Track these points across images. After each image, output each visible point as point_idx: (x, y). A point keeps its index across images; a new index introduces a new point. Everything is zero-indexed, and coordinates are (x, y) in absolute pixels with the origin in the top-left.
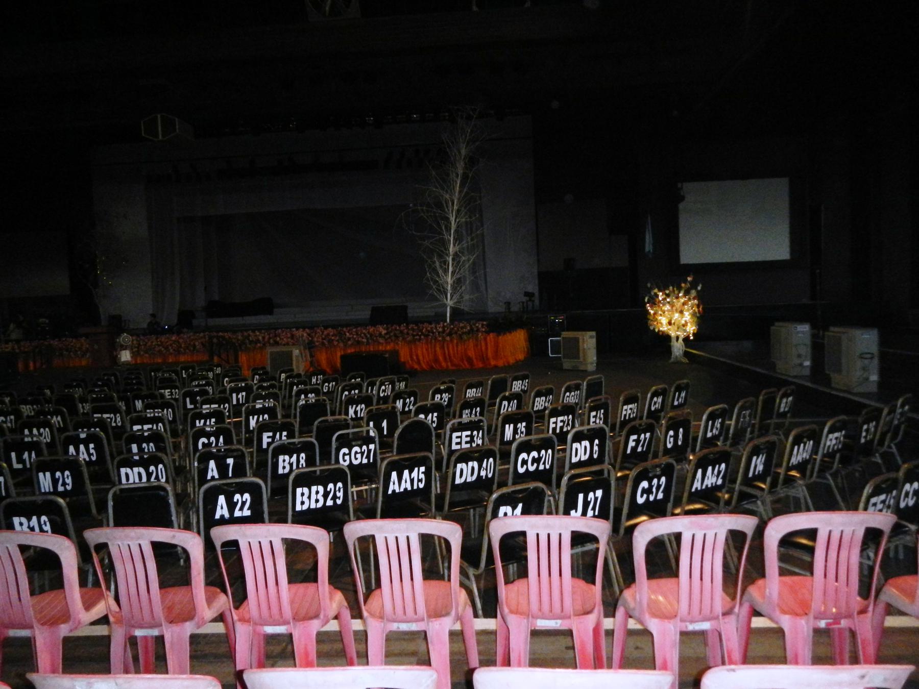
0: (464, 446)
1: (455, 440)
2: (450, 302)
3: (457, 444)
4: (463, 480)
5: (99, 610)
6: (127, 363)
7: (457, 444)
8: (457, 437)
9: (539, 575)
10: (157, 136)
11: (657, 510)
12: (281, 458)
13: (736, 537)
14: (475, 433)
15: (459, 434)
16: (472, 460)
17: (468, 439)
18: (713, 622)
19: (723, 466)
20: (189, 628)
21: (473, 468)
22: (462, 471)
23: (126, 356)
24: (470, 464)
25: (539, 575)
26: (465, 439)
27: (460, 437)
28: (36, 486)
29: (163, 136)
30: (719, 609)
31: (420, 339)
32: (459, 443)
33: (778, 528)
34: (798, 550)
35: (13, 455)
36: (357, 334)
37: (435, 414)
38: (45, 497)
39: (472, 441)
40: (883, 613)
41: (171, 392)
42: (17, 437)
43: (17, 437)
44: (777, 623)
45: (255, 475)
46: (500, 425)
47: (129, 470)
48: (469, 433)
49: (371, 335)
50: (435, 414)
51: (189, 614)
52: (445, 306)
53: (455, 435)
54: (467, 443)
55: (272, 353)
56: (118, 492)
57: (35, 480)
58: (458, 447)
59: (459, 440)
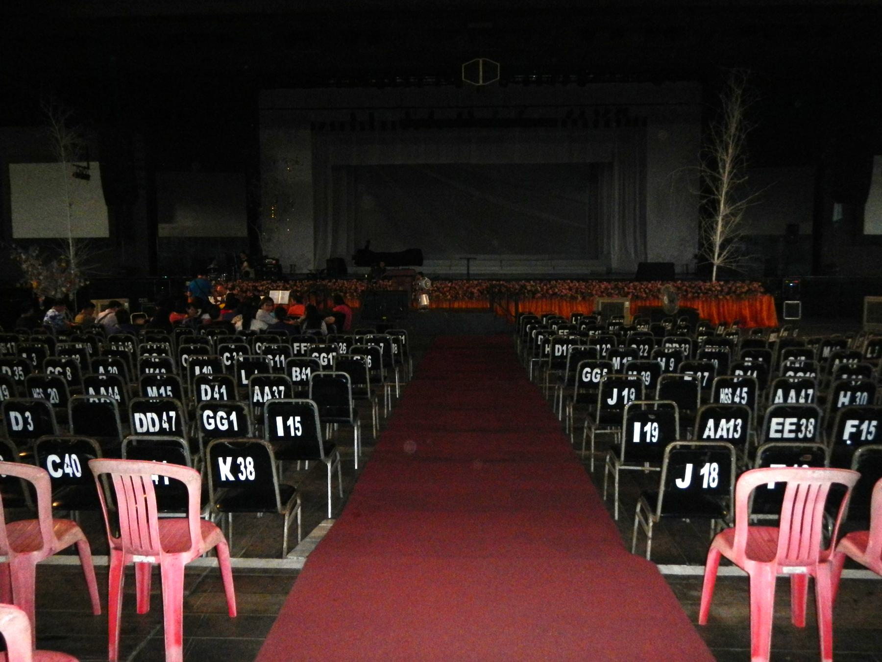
0: (786, 435)
2: (717, 261)
3: (777, 431)
5: (67, 541)
6: (425, 307)
7: (777, 431)
8: (778, 424)
12: (294, 369)
13: (836, 492)
14: (804, 421)
15: (781, 420)
17: (794, 427)
18: (810, 567)
20: (186, 558)
22: (141, 420)
23: (425, 300)
26: (787, 427)
27: (783, 424)
28: (132, 427)
30: (816, 555)
31: (698, 297)
36: (635, 289)
37: (874, 423)
38: (140, 438)
39: (798, 429)
41: (798, 426)
42: (105, 358)
43: (105, 358)
44: (878, 574)
45: (313, 399)
46: (837, 420)
47: (142, 416)
48: (795, 420)
49: (650, 291)
50: (874, 423)
51: (184, 545)
52: (712, 265)
53: (775, 420)
54: (790, 431)
57: (131, 420)
58: (779, 435)
59: (780, 427)
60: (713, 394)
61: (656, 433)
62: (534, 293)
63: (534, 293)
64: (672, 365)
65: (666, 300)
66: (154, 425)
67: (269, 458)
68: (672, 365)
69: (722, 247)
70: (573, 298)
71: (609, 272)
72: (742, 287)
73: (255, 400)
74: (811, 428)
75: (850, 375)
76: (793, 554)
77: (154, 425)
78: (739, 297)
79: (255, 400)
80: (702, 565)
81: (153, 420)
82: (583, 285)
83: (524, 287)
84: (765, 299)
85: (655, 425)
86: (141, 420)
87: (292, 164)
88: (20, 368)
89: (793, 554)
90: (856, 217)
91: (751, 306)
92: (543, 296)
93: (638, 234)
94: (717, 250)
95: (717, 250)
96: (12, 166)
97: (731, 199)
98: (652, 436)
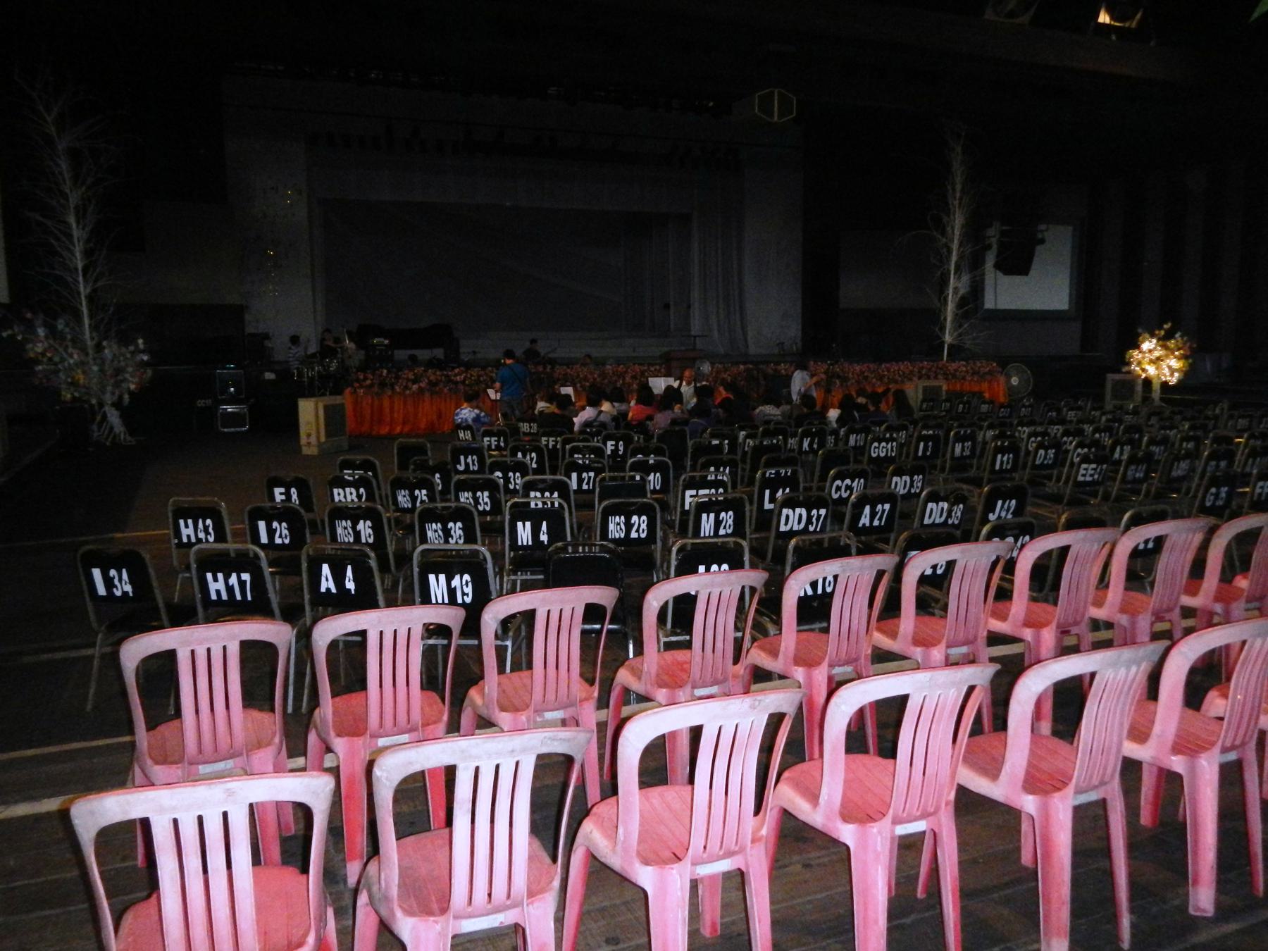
1: (1082, 472)
2: (948, 338)
4: (931, 521)
9: (381, 686)
10: (772, 116)
11: (343, 603)
13: (593, 613)
16: (943, 500)
19: (1014, 502)
21: (800, 516)
22: (787, 517)
24: (798, 510)
25: (381, 686)
29: (780, 116)
32: (1084, 475)
33: (797, 585)
34: (935, 588)
35: (767, 492)
40: (747, 677)
47: (791, 512)
52: (943, 343)
55: (940, 387)
56: (689, 548)
60: (84, 583)
61: (469, 590)
64: (621, 448)
66: (799, 522)
68: (621, 448)
73: (323, 590)
74: (644, 526)
76: (551, 696)
77: (799, 522)
79: (323, 590)
80: (283, 859)
81: (800, 516)
85: (467, 577)
86: (787, 517)
87: (282, 197)
88: (424, 492)
89: (551, 696)
98: (464, 594)
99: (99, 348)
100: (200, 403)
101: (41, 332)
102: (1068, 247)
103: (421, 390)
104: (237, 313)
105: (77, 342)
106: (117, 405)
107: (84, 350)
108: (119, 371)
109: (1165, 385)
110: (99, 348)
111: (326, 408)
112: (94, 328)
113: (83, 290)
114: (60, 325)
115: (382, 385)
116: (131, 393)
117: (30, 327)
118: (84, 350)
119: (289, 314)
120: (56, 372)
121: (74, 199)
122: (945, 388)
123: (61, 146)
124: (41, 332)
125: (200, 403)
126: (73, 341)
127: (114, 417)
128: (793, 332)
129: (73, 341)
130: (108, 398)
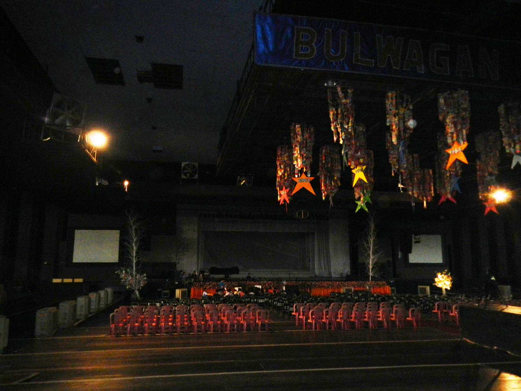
2: (371, 274)
52: (369, 276)
62: (315, 286)
63: (315, 286)
65: (367, 287)
67: (269, 347)
69: (372, 269)
70: (328, 287)
71: (316, 277)
72: (380, 283)
75: (184, 317)
78: (380, 287)
82: (331, 283)
83: (311, 283)
84: (388, 287)
87: (190, 232)
90: (406, 258)
91: (384, 289)
92: (319, 287)
93: (326, 262)
94: (371, 270)
95: (371, 270)
96: (76, 231)
97: (374, 254)
99: (136, 276)
100: (159, 290)
101: (124, 272)
102: (440, 240)
103: (210, 287)
104: (174, 265)
105: (132, 274)
106: (138, 290)
107: (132, 276)
108: (140, 281)
109: (446, 290)
110: (136, 276)
111: (182, 292)
112: (136, 271)
113: (134, 261)
114: (128, 270)
115: (201, 286)
116: (142, 287)
117: (122, 271)
118: (132, 276)
119: (189, 264)
120: (126, 281)
121: (135, 240)
122: (353, 289)
123: (134, 227)
124: (124, 272)
125: (159, 290)
126: (131, 274)
127: (137, 293)
128: (347, 270)
129: (131, 274)
130: (136, 288)
